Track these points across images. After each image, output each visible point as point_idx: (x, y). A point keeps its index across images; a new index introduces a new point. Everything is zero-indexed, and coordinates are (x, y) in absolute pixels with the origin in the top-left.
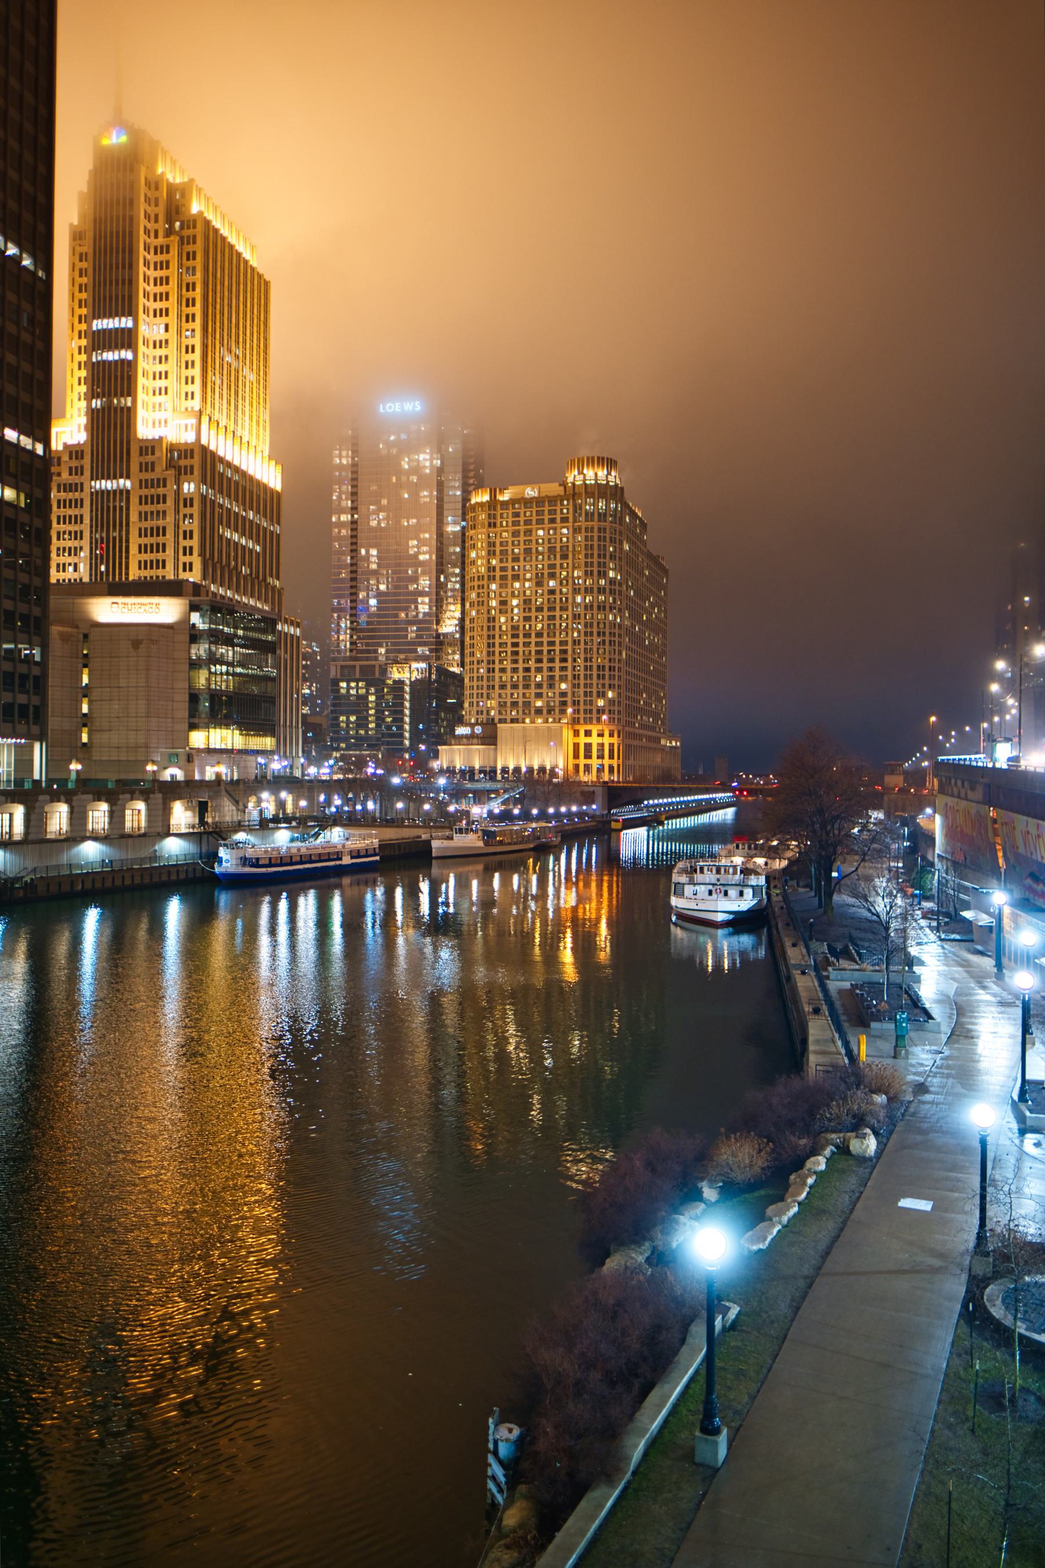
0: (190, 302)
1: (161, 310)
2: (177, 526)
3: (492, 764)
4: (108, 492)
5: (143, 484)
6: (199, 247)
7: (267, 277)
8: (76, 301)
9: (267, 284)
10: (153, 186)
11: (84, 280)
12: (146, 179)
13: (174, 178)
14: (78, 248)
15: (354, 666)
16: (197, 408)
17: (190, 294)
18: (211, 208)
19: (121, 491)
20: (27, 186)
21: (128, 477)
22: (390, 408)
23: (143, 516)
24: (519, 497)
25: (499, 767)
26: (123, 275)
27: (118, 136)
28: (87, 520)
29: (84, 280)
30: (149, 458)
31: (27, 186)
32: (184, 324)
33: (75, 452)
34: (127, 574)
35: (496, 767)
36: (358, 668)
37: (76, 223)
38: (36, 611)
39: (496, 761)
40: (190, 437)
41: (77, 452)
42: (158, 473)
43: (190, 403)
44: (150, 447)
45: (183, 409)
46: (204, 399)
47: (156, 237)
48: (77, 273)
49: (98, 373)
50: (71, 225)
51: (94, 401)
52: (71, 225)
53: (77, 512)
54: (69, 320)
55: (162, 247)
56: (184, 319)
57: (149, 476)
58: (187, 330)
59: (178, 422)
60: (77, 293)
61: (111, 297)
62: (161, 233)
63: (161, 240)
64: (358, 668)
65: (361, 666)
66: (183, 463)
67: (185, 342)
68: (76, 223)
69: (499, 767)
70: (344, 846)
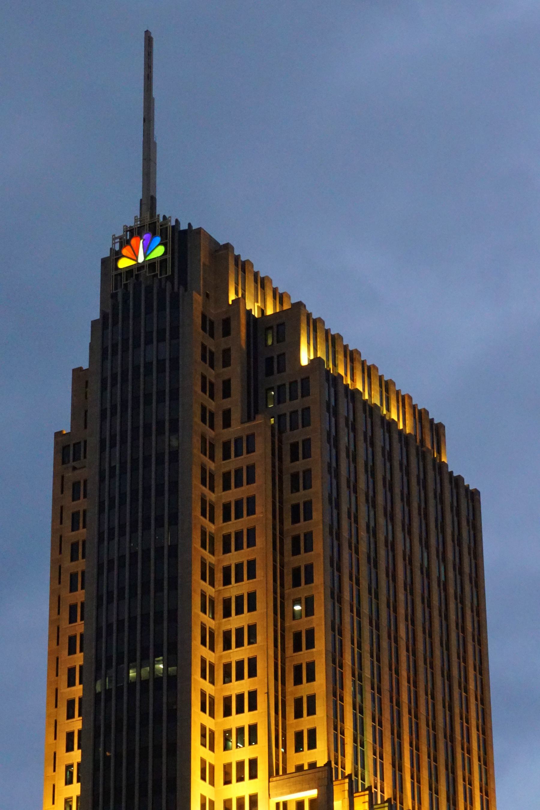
7: (471, 482)
11: (80, 565)
12: (204, 317)
13: (263, 311)
14: (70, 476)
16: (321, 763)
18: (340, 357)
29: (80, 565)
32: (289, 590)
37: (67, 429)
45: (291, 769)
47: (227, 424)
50: (59, 435)
51: (99, 683)
52: (59, 435)
54: (49, 683)
55: (238, 441)
56: (289, 579)
58: (297, 601)
59: (281, 799)
60: (65, 592)
62: (236, 416)
65: (167, 242)
67: (291, 625)
68: (67, 429)
70: (135, 225)
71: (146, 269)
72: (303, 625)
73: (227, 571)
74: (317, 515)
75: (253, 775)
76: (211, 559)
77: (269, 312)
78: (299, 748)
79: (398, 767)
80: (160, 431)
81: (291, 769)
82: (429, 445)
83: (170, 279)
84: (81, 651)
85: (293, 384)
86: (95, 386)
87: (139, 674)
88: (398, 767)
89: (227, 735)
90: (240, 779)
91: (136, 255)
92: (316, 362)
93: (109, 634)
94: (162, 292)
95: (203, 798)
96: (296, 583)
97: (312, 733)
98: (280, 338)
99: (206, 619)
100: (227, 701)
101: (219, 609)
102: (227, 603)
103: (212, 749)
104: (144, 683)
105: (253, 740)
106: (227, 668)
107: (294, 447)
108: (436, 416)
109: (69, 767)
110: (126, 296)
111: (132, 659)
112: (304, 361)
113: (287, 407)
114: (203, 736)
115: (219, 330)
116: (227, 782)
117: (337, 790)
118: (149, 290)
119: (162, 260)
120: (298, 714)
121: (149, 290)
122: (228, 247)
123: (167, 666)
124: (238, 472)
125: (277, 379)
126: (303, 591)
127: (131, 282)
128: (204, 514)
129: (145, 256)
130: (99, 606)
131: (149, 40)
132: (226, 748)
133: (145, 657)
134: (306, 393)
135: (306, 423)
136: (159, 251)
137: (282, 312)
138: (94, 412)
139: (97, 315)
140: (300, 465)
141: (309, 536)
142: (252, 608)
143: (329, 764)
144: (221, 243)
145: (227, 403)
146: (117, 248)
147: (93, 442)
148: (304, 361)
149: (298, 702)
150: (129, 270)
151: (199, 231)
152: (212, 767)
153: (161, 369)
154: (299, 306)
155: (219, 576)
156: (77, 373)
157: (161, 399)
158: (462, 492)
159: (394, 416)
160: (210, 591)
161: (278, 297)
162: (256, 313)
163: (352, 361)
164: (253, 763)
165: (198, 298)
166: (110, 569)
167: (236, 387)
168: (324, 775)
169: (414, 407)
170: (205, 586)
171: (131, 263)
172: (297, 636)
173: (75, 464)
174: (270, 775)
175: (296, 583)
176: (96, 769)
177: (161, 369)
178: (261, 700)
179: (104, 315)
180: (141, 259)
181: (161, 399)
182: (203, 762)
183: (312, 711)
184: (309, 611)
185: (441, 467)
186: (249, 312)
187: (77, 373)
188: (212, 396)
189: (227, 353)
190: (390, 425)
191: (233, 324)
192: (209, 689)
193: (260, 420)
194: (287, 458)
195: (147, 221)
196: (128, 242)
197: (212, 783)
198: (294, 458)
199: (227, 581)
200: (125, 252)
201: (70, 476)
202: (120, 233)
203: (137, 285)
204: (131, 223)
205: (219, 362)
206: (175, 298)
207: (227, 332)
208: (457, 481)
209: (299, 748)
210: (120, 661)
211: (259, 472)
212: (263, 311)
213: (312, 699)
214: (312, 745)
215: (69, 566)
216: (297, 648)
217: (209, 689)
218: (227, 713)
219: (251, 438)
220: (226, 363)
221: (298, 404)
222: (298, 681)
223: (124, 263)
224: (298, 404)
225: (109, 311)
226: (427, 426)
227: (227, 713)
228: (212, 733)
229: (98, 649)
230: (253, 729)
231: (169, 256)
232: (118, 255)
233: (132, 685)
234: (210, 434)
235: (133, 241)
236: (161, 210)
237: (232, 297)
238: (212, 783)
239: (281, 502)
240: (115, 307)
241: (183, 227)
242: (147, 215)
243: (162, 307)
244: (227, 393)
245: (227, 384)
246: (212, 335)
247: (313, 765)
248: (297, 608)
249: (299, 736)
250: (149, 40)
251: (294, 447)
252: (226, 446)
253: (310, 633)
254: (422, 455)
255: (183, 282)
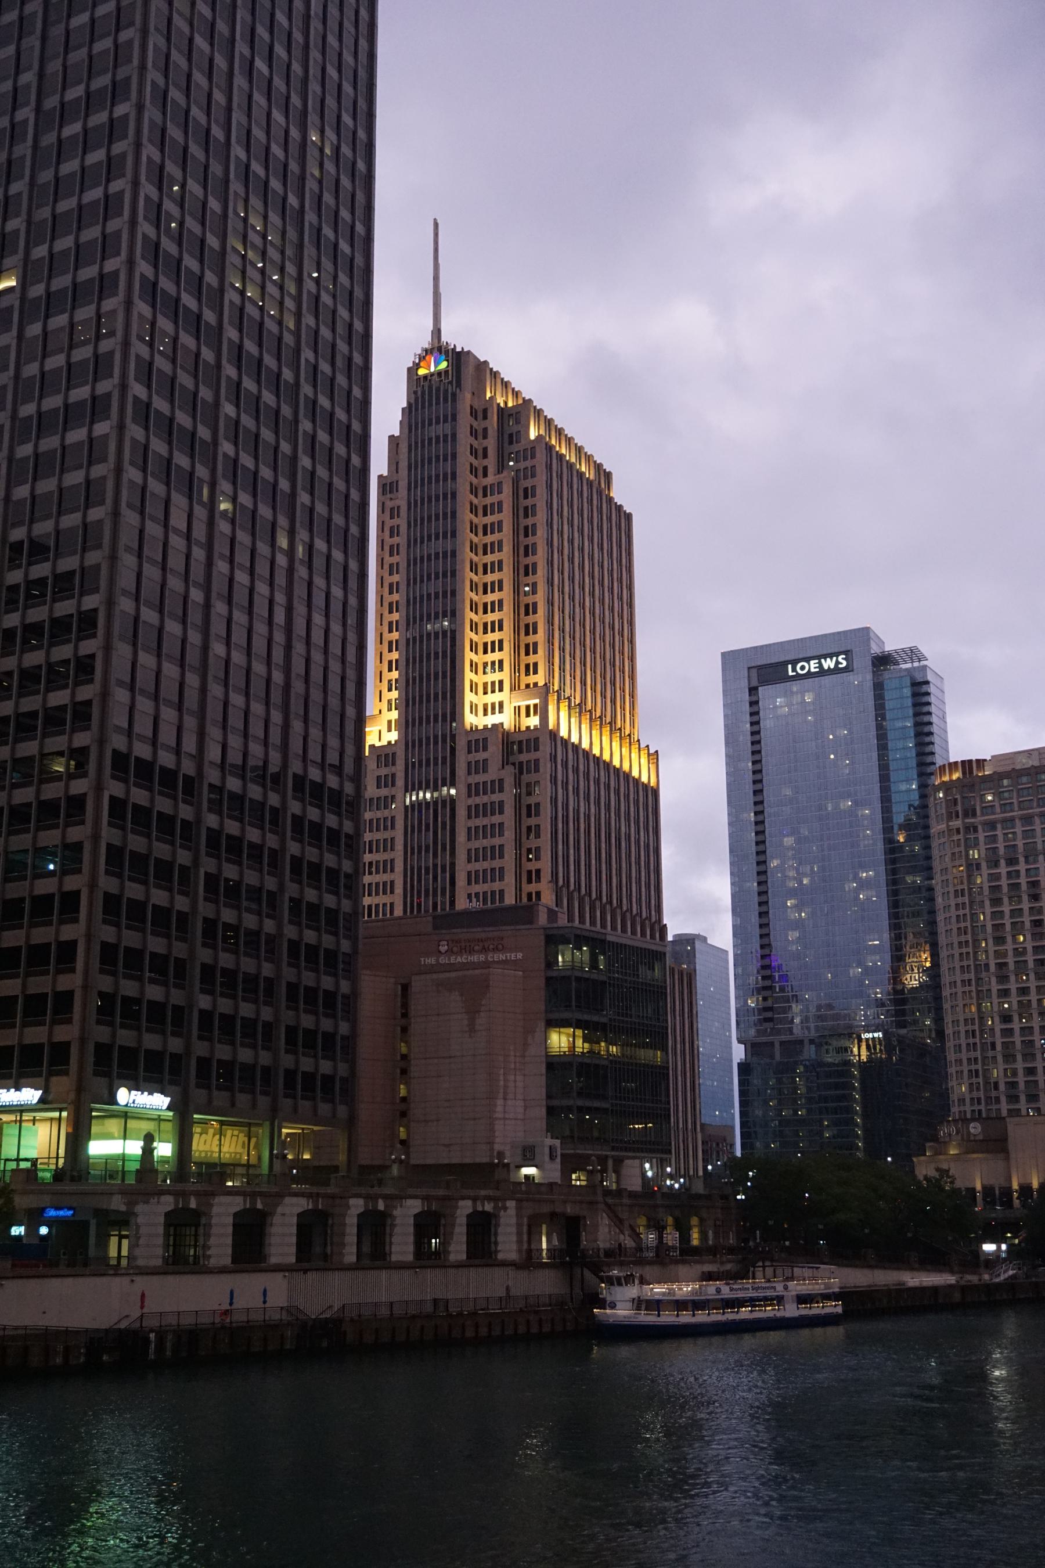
0: (531, 649)
1: (493, 705)
2: (519, 865)
3: (1004, 1184)
4: (427, 804)
5: (472, 790)
6: (545, 820)
7: (627, 509)
8: (386, 605)
9: (629, 517)
10: (480, 453)
13: (506, 403)
15: (772, 1044)
16: (541, 684)
17: (530, 619)
18: (553, 433)
19: (444, 802)
20: (341, 415)
21: (453, 784)
22: (803, 668)
23: (472, 833)
24: (1009, 768)
25: (1015, 1186)
26: (436, 708)
27: (436, 365)
28: (399, 889)
30: (481, 756)
31: (341, 415)
33: (385, 755)
34: (452, 903)
35: (1011, 1187)
36: (777, 1045)
37: (385, 474)
38: (348, 827)
39: (1009, 1179)
40: (534, 721)
41: (387, 755)
42: (493, 773)
43: (532, 679)
44: (481, 739)
45: (523, 686)
46: (550, 672)
47: (485, 475)
48: (386, 589)
49: (414, 652)
53: (387, 835)
57: (480, 778)
58: (527, 585)
59: (517, 704)
61: (420, 741)
63: (491, 479)
64: (777, 1045)
65: (782, 1043)
66: (524, 757)
69: (1015, 1186)
71: (436, 376)
72: (530, 600)
73: (485, 566)
74: (540, 572)
75: (501, 690)
76: (475, 559)
77: (510, 404)
78: (527, 673)
79: (584, 683)
80: (445, 479)
81: (523, 686)
82: (603, 486)
83: (451, 383)
84: (397, 630)
85: (525, 450)
86: (404, 448)
87: (432, 796)
88: (584, 683)
89: (485, 665)
90: (493, 691)
91: (429, 366)
92: (539, 437)
93: (415, 603)
94: (446, 391)
95: (471, 703)
96: (527, 574)
97: (536, 665)
98: (517, 422)
99: (473, 595)
100: (485, 645)
101: (481, 589)
102: (485, 585)
103: (476, 653)
104: (436, 634)
105: (501, 669)
106: (485, 625)
107: (526, 490)
108: (607, 467)
109: (390, 681)
110: (423, 393)
111: (429, 619)
112: (532, 436)
113: (522, 465)
114: (471, 665)
115: (480, 415)
116: (485, 693)
117: (550, 698)
118: (438, 390)
119: (446, 372)
120: (527, 654)
121: (438, 390)
122: (486, 363)
123: (450, 623)
124: (493, 544)
125: (515, 448)
126: (531, 579)
127: (427, 384)
128: (471, 531)
129: (436, 366)
130: (408, 585)
131: (436, 225)
132: (485, 673)
133: (437, 617)
134: (533, 457)
135: (533, 476)
136: (444, 365)
137: (518, 405)
138: (404, 464)
139: (405, 405)
140: (529, 502)
141: (535, 625)
142: (500, 609)
143: (546, 684)
144: (482, 360)
145: (485, 462)
146: (417, 361)
147: (403, 484)
148: (532, 436)
149: (527, 646)
150: (425, 377)
151: (469, 352)
152: (476, 684)
153: (445, 441)
154: (528, 402)
155: (480, 569)
156: (391, 438)
157: (445, 460)
158: (622, 514)
159: (583, 469)
160: (475, 578)
161: (516, 394)
162: (502, 405)
163: (560, 434)
164: (501, 682)
165: (468, 396)
166: (415, 564)
167: (492, 453)
168: (544, 690)
169: (595, 462)
170: (472, 575)
171: (426, 372)
172: (527, 606)
173: (392, 496)
174: (511, 690)
175: (527, 574)
176: (407, 722)
177: (445, 441)
178: (506, 645)
179: (409, 403)
180: (432, 369)
181: (445, 460)
182: (471, 681)
183: (535, 652)
184: (534, 591)
185: (610, 500)
186: (499, 405)
187: (391, 438)
188: (476, 458)
189: (485, 430)
190: (581, 475)
191: (489, 414)
192: (475, 618)
193: (505, 473)
194: (524, 837)
195: (436, 345)
196: (424, 358)
197: (476, 693)
198: (526, 497)
199: (485, 572)
200: (422, 364)
201: (389, 504)
202: (419, 352)
203: (430, 387)
204: (426, 346)
205: (480, 437)
206: (454, 395)
207: (485, 417)
208: (619, 508)
209: (527, 673)
210: (421, 620)
211: (505, 506)
212: (506, 403)
213: (535, 644)
214: (535, 672)
215: (388, 560)
216: (527, 614)
217: (475, 638)
218: (485, 652)
219: (500, 484)
220: (485, 437)
221: (528, 463)
222: (527, 634)
223: (422, 372)
224: (528, 463)
225: (412, 401)
226: (602, 473)
227: (485, 652)
228: (476, 664)
229: (407, 651)
230: (501, 662)
231: (450, 368)
232: (417, 366)
233: (429, 635)
234: (475, 481)
235: (427, 358)
236: (444, 339)
237: (488, 395)
238: (476, 693)
239: (521, 890)
240: (416, 400)
241: (459, 349)
242: (436, 341)
243: (446, 400)
244: (485, 456)
245: (485, 450)
246: (476, 419)
247: (536, 684)
248: (527, 589)
249: (527, 666)
250: (436, 225)
251: (526, 490)
252: (485, 488)
253: (535, 604)
254: (600, 493)
255: (459, 384)
